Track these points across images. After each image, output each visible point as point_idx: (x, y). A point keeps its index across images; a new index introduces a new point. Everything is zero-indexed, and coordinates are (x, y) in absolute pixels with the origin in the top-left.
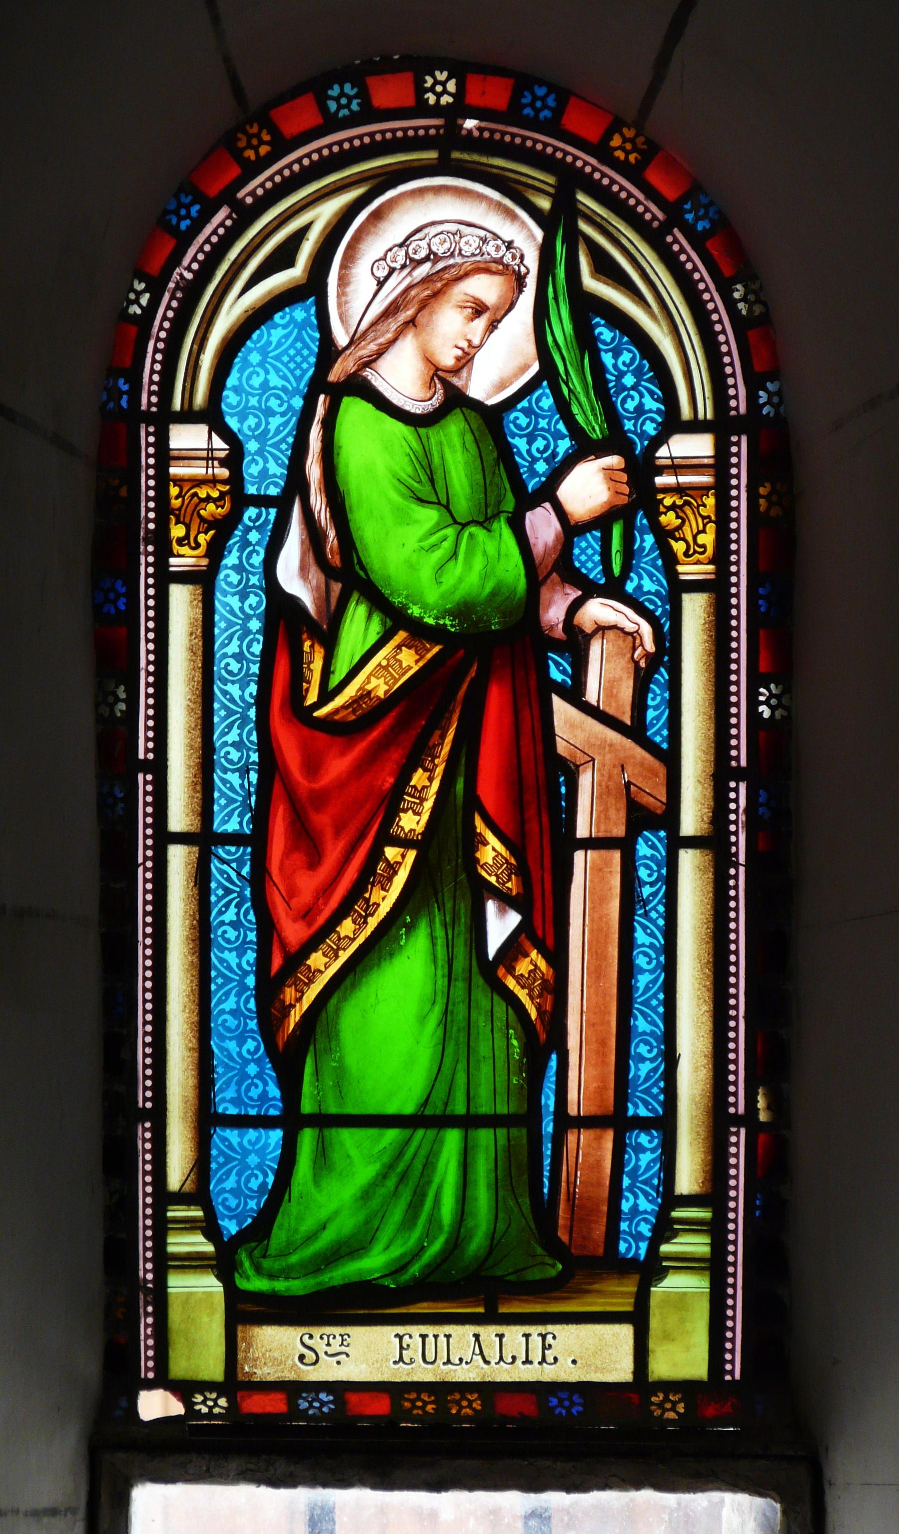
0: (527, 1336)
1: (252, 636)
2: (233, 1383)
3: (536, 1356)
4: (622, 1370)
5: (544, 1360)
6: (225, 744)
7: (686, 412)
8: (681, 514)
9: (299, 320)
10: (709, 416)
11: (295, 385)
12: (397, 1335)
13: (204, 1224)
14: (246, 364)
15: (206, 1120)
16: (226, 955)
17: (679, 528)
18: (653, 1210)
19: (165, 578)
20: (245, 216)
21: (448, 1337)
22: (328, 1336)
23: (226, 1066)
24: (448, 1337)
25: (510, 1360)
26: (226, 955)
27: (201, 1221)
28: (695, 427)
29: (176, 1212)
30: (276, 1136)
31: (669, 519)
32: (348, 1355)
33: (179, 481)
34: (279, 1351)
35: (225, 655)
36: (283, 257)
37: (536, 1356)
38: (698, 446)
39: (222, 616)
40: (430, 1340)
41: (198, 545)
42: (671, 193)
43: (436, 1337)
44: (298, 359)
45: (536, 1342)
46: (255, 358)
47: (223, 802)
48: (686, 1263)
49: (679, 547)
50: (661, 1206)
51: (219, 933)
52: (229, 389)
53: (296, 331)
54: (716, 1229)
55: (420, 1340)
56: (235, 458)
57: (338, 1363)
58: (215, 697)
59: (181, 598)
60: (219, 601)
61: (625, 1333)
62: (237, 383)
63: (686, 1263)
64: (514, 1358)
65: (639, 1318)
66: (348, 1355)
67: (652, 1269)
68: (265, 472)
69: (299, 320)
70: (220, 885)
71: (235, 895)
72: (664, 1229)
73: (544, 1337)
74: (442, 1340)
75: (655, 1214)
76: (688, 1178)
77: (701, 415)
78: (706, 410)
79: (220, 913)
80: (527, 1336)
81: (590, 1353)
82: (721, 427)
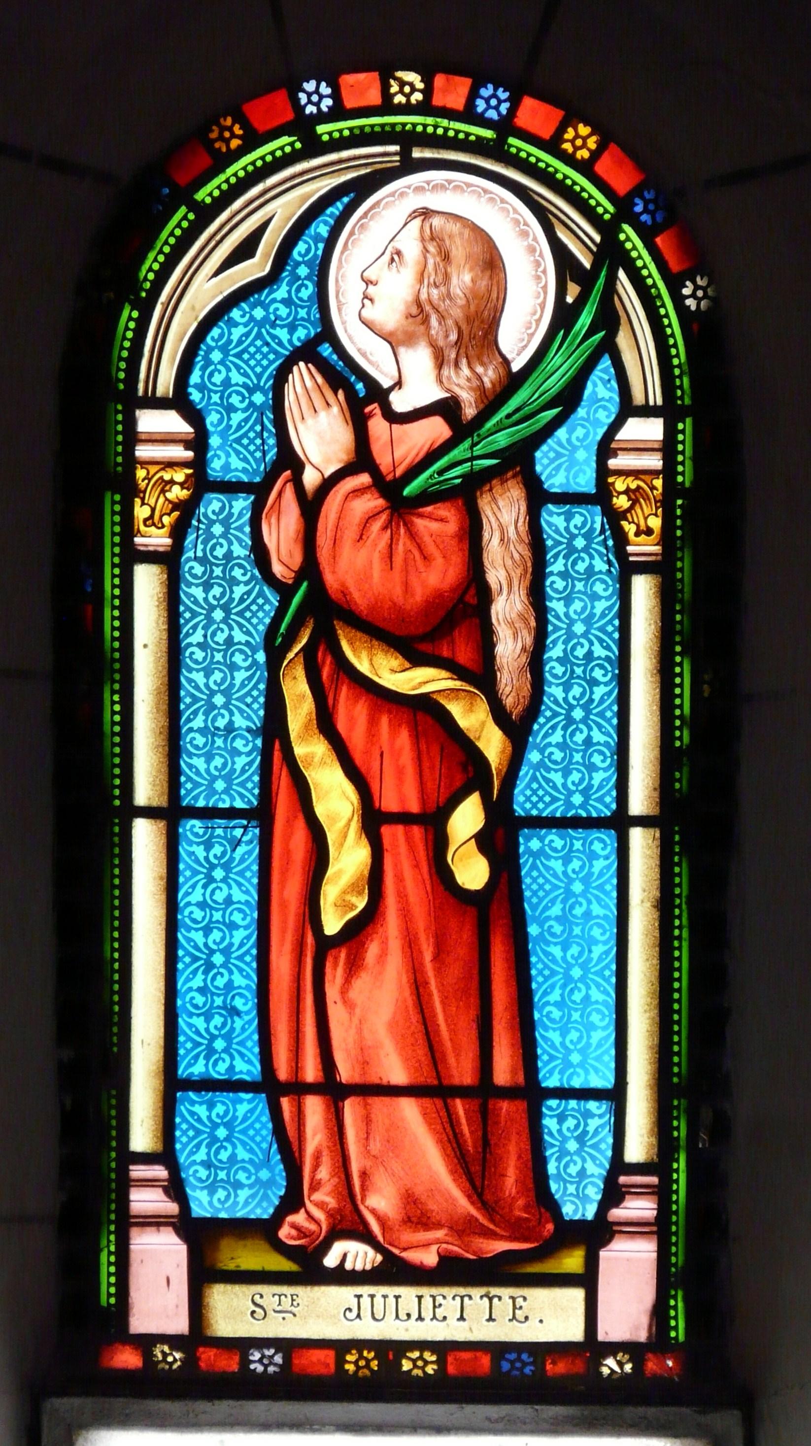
0: (420, 1298)
1: (215, 541)
2: (197, 1335)
3: (427, 1313)
4: (575, 1332)
5: (434, 1317)
6: (190, 989)
7: (638, 398)
8: (633, 497)
9: (259, 318)
10: (660, 402)
11: (255, 382)
12: (432, 1296)
13: (166, 1183)
14: (208, 362)
15: (173, 1085)
16: (193, 935)
17: (629, 510)
18: (600, 1174)
19: (132, 556)
20: (206, 214)
21: (397, 1297)
22: (462, 1298)
23: (192, 696)
24: (397, 1297)
25: (406, 1318)
26: (193, 935)
27: (163, 1181)
28: (646, 411)
29: (138, 1171)
30: (248, 1068)
31: (622, 502)
32: (295, 1315)
33: (145, 463)
34: (233, 1312)
35: (189, 904)
36: (245, 250)
37: (427, 1313)
38: (651, 430)
39: (188, 692)
40: (378, 1300)
41: (163, 526)
42: (622, 186)
43: (372, 1296)
44: (258, 357)
45: (427, 1302)
46: (216, 356)
47: (189, 1045)
48: (636, 1228)
49: (630, 529)
50: (609, 1172)
51: (191, 1172)
52: (192, 386)
53: (256, 329)
54: (663, 1194)
55: (394, 1300)
56: (199, 442)
57: (284, 1319)
58: (181, 859)
59: (147, 581)
60: (185, 762)
61: (577, 1295)
62: (199, 381)
63: (636, 1228)
64: (409, 1315)
65: (588, 1280)
66: (295, 1315)
67: (596, 1234)
68: (227, 461)
69: (259, 318)
70: (188, 953)
71: (202, 617)
72: (613, 1194)
73: (434, 1297)
74: (391, 1301)
75: (602, 1178)
76: (638, 1147)
77: (651, 403)
78: (656, 398)
79: (188, 980)
80: (420, 1298)
81: (550, 1316)
82: (669, 411)
